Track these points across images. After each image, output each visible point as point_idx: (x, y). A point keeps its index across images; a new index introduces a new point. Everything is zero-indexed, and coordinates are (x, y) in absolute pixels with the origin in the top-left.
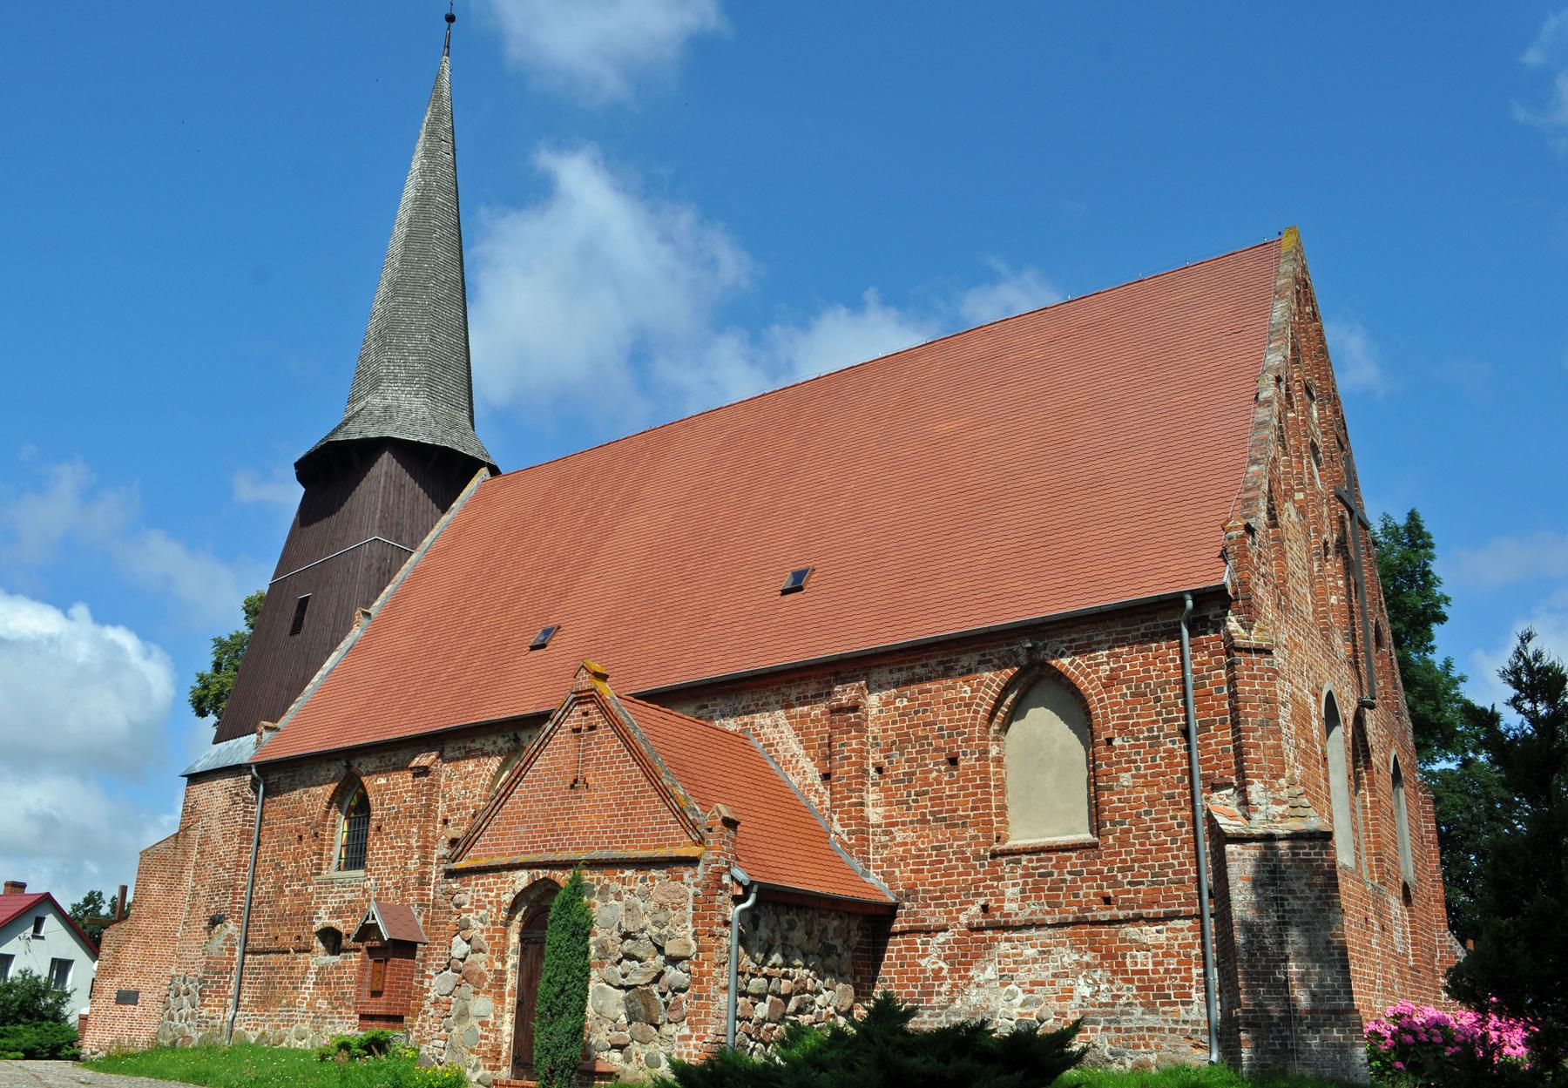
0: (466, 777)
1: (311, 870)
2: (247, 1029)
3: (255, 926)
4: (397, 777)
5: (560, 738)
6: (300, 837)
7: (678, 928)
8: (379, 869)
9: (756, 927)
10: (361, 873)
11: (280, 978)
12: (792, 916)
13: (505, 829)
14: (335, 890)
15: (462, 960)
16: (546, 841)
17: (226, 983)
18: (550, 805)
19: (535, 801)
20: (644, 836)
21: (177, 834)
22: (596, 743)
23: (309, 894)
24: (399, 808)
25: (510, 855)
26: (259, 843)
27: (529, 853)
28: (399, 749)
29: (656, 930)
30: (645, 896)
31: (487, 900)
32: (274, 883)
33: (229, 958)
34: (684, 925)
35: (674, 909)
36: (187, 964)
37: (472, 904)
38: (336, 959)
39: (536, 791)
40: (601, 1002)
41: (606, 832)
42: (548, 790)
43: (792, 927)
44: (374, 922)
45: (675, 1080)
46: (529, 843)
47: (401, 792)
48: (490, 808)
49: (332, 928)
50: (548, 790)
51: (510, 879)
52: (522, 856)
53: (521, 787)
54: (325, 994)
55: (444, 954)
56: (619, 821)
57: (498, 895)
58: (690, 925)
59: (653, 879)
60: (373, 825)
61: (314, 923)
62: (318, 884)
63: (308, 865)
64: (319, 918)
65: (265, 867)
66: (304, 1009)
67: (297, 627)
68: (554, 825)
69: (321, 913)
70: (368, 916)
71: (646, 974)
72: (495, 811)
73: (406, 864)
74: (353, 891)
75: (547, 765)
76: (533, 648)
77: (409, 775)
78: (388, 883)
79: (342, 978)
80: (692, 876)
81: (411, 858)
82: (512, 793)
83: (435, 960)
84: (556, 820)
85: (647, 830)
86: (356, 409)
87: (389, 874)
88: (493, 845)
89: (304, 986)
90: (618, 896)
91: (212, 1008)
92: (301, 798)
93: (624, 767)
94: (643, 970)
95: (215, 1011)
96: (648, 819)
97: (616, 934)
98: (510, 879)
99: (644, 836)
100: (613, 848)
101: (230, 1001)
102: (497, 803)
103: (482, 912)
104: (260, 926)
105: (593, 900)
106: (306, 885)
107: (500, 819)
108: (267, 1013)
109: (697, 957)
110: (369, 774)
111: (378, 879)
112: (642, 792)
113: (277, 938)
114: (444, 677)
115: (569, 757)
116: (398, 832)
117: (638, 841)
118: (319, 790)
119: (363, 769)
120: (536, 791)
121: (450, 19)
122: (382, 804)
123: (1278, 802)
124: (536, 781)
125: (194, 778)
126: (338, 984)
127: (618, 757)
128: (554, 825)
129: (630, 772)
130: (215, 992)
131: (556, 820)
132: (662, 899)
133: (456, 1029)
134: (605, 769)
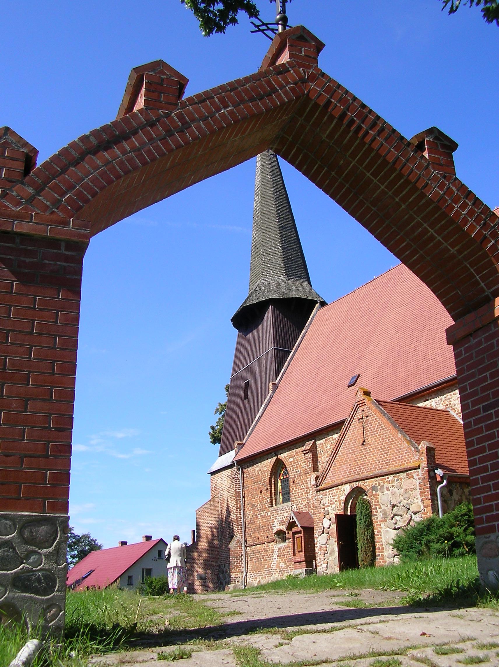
0: (328, 452)
1: (268, 505)
2: (252, 581)
3: (248, 534)
5: (354, 424)
6: (261, 492)
7: (415, 499)
8: (297, 500)
9: (451, 495)
11: (263, 556)
13: (338, 468)
14: (280, 512)
15: (329, 528)
16: (355, 470)
17: (240, 561)
18: (355, 454)
19: (348, 454)
20: (395, 461)
21: (210, 500)
22: (369, 423)
23: (269, 516)
24: (301, 471)
25: (341, 479)
26: (244, 497)
27: (349, 477)
28: (296, 443)
29: (405, 501)
30: (399, 487)
31: (334, 500)
32: (253, 514)
33: (240, 550)
34: (417, 497)
35: (412, 491)
36: (225, 558)
37: (329, 503)
38: (285, 544)
39: (348, 449)
40: (387, 537)
41: (379, 462)
42: (353, 448)
44: (293, 520)
46: (348, 472)
47: (300, 463)
48: (330, 460)
49: (281, 530)
50: (353, 448)
51: (343, 489)
52: (346, 479)
53: (342, 448)
54: (283, 560)
55: (321, 527)
56: (384, 456)
57: (339, 497)
58: (419, 497)
59: (401, 479)
60: (291, 480)
61: (273, 529)
62: (272, 511)
63: (266, 503)
64: (275, 526)
65: (248, 507)
66: (275, 568)
67: (246, 397)
68: (358, 463)
69: (275, 524)
70: (290, 518)
71: (404, 521)
72: (332, 461)
73: (308, 496)
74: (287, 512)
75: (350, 437)
76: (349, 386)
78: (302, 506)
79: (289, 552)
80: (417, 475)
81: (309, 492)
82: (338, 452)
83: (317, 530)
84: (358, 460)
85: (396, 458)
86: (254, 288)
87: (301, 501)
88: (334, 476)
89: (273, 558)
90: (388, 489)
91: (236, 573)
92: (258, 473)
93: (383, 432)
94: (403, 520)
95: (237, 574)
96: (396, 453)
97: (389, 506)
98: (343, 489)
99: (395, 461)
100: (383, 468)
101: (244, 569)
102: (333, 457)
103: (333, 506)
104: (251, 534)
105: (378, 493)
106: (267, 512)
107: (335, 464)
108: (259, 573)
109: (424, 511)
111: (297, 505)
112: (392, 441)
113: (258, 538)
114: (312, 407)
115: (359, 432)
116: (302, 482)
117: (393, 464)
120: (348, 449)
122: (293, 470)
124: (347, 444)
125: (213, 473)
126: (288, 555)
127: (379, 428)
128: (358, 463)
129: (385, 433)
130: (236, 566)
131: (358, 460)
132: (406, 487)
133: (330, 558)
134: (375, 434)
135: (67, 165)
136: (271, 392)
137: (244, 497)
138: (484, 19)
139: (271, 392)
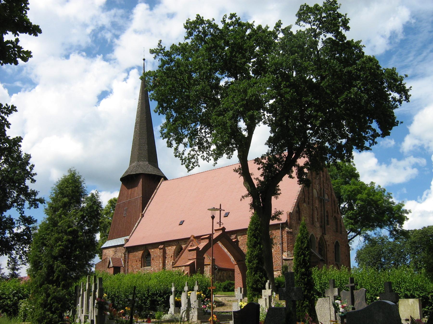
4: (156, 250)
6: (137, 261)
10: (150, 267)
12: (224, 272)
43: (224, 273)
45: (111, 56)
60: (152, 258)
77: (158, 249)
110: (150, 249)
118: (140, 252)
119: (149, 248)
121: (144, 60)
123: (291, 254)
135: (281, 100)
136: (140, 218)
137: (128, 262)
138: (8, 34)
139: (140, 218)
